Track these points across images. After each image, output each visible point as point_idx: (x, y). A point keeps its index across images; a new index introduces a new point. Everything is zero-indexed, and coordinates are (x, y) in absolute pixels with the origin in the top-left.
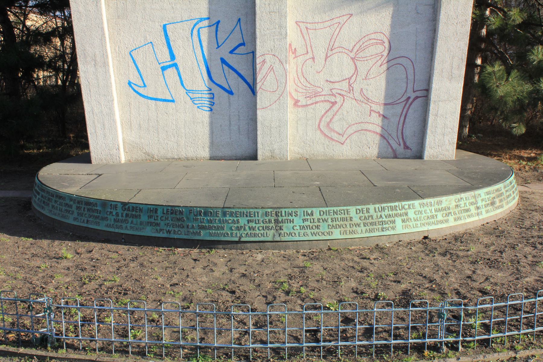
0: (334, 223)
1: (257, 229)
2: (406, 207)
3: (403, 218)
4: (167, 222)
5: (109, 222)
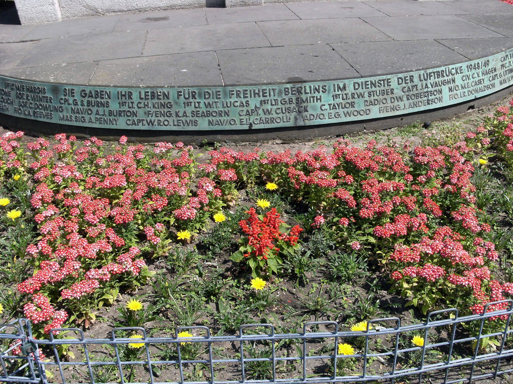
0: (372, 98)
1: (273, 112)
2: (454, 71)
3: (450, 85)
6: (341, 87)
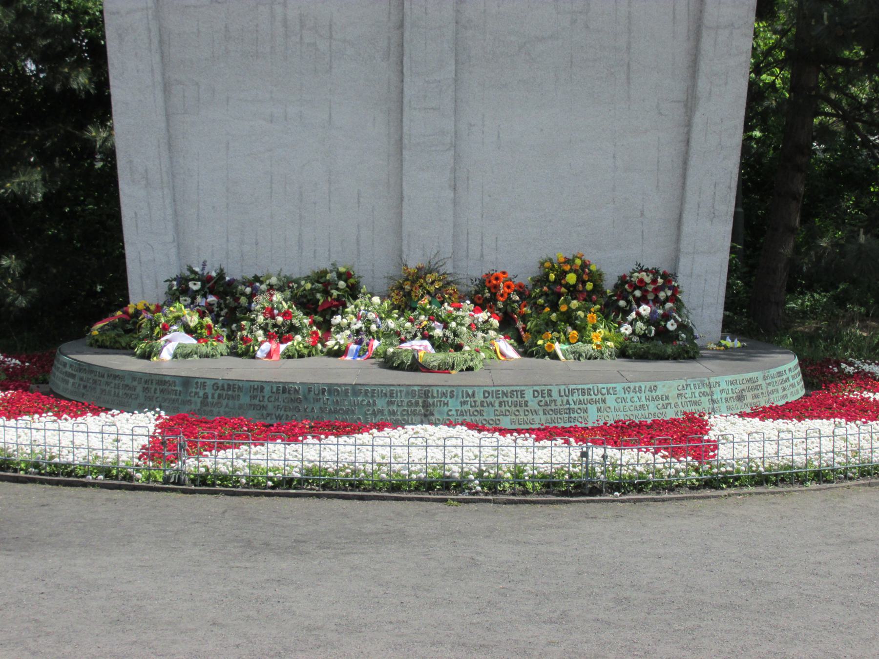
0: (503, 409)
4: (277, 403)
5: (193, 406)
6: (470, 393)
